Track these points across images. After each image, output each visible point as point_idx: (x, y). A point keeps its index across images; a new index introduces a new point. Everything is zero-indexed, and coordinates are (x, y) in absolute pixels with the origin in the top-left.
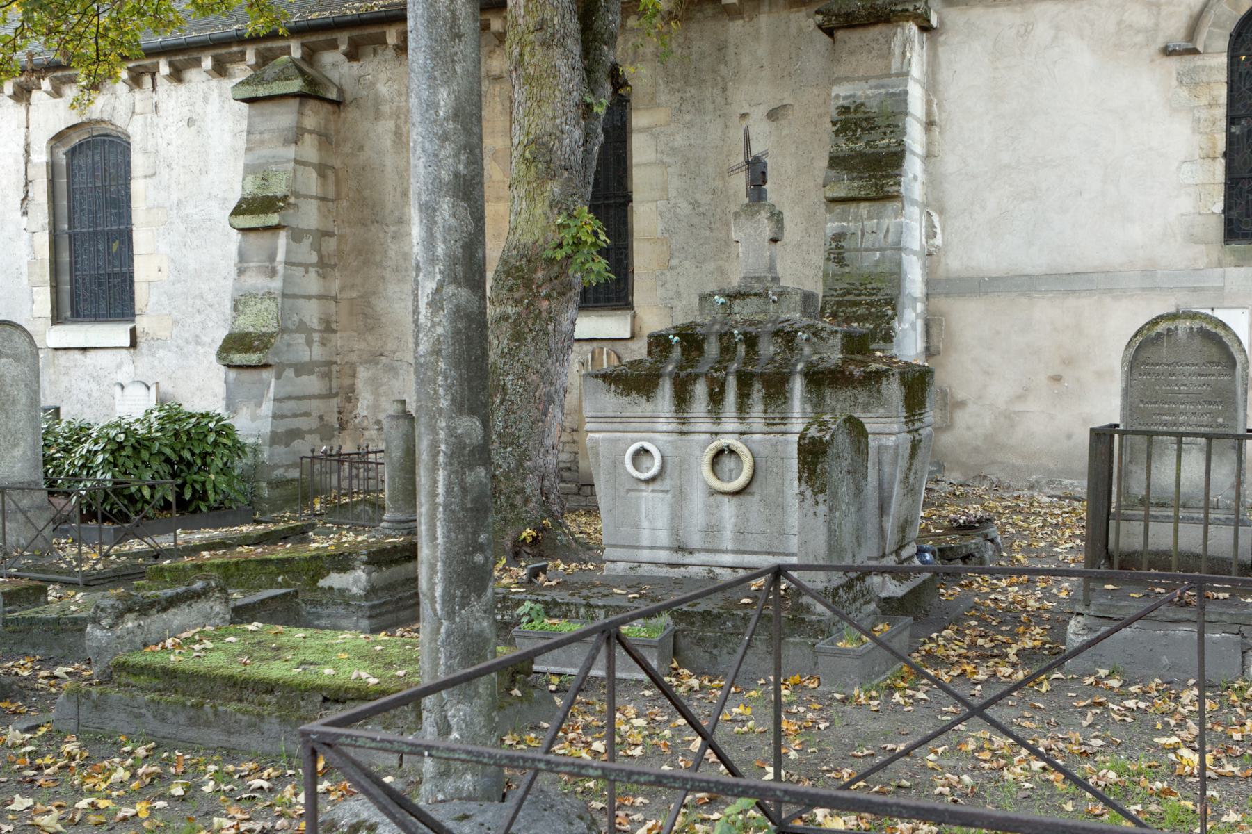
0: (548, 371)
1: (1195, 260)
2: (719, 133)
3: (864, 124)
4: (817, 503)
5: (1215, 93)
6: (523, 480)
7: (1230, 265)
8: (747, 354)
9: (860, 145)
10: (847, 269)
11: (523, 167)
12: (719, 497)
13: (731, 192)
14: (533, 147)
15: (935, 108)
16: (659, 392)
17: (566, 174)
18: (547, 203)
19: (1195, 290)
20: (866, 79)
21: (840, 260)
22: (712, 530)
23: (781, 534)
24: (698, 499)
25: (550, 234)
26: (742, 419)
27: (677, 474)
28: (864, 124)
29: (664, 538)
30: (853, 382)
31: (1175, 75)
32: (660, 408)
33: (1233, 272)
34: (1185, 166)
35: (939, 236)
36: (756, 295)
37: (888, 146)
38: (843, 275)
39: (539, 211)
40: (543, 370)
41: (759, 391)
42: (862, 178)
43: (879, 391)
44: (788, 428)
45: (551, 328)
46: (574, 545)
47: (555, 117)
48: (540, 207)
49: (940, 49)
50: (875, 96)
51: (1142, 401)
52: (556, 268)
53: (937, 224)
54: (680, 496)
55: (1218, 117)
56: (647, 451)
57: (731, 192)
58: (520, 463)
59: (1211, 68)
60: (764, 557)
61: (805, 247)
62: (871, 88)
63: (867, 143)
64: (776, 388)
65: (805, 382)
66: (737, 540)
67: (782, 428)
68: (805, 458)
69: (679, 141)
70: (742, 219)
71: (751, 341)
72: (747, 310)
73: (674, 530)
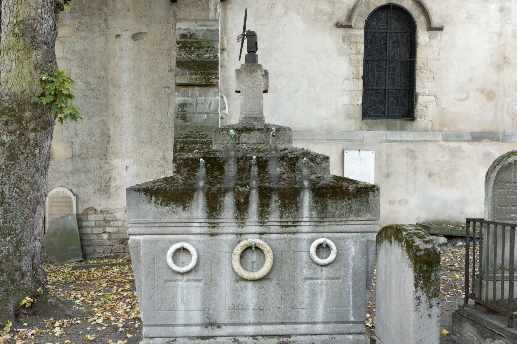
0: (36, 181)
1: (350, 126)
2: (103, 44)
4: (431, 306)
5: (359, 48)
6: (20, 260)
7: (365, 130)
8: (259, 174)
9: (194, 56)
10: (188, 123)
11: (14, 40)
12: (243, 283)
14: (21, 26)
15: (225, 42)
16: (194, 203)
17: (45, 47)
18: (32, 65)
19: (351, 141)
20: (196, 21)
21: (184, 118)
22: (237, 309)
23: (292, 308)
24: (226, 284)
25: (35, 87)
26: (262, 223)
27: (208, 266)
28: (195, 45)
29: (197, 317)
30: (348, 195)
32: (195, 215)
33: (367, 133)
34: (345, 81)
35: (227, 109)
36: (259, 130)
37: (209, 58)
38: (186, 126)
39: (25, 71)
40: (32, 181)
41: (276, 201)
42: (197, 74)
43: (367, 201)
44: (299, 228)
45: (37, 151)
46: (61, 305)
47: (37, 8)
48: (27, 68)
49: (228, 11)
50: (201, 30)
51: (499, 205)
52: (39, 111)
53: (226, 102)
54: (211, 283)
55: (360, 59)
56: (185, 250)
57: (110, 78)
58: (17, 248)
59: (357, 36)
60: (279, 326)
61: (153, 111)
62: (198, 26)
63: (197, 55)
64: (290, 199)
66: (257, 315)
67: (293, 229)
68: (421, 267)
69: (78, 46)
70: (243, 75)
71: (262, 164)
72: (252, 141)
73: (205, 311)
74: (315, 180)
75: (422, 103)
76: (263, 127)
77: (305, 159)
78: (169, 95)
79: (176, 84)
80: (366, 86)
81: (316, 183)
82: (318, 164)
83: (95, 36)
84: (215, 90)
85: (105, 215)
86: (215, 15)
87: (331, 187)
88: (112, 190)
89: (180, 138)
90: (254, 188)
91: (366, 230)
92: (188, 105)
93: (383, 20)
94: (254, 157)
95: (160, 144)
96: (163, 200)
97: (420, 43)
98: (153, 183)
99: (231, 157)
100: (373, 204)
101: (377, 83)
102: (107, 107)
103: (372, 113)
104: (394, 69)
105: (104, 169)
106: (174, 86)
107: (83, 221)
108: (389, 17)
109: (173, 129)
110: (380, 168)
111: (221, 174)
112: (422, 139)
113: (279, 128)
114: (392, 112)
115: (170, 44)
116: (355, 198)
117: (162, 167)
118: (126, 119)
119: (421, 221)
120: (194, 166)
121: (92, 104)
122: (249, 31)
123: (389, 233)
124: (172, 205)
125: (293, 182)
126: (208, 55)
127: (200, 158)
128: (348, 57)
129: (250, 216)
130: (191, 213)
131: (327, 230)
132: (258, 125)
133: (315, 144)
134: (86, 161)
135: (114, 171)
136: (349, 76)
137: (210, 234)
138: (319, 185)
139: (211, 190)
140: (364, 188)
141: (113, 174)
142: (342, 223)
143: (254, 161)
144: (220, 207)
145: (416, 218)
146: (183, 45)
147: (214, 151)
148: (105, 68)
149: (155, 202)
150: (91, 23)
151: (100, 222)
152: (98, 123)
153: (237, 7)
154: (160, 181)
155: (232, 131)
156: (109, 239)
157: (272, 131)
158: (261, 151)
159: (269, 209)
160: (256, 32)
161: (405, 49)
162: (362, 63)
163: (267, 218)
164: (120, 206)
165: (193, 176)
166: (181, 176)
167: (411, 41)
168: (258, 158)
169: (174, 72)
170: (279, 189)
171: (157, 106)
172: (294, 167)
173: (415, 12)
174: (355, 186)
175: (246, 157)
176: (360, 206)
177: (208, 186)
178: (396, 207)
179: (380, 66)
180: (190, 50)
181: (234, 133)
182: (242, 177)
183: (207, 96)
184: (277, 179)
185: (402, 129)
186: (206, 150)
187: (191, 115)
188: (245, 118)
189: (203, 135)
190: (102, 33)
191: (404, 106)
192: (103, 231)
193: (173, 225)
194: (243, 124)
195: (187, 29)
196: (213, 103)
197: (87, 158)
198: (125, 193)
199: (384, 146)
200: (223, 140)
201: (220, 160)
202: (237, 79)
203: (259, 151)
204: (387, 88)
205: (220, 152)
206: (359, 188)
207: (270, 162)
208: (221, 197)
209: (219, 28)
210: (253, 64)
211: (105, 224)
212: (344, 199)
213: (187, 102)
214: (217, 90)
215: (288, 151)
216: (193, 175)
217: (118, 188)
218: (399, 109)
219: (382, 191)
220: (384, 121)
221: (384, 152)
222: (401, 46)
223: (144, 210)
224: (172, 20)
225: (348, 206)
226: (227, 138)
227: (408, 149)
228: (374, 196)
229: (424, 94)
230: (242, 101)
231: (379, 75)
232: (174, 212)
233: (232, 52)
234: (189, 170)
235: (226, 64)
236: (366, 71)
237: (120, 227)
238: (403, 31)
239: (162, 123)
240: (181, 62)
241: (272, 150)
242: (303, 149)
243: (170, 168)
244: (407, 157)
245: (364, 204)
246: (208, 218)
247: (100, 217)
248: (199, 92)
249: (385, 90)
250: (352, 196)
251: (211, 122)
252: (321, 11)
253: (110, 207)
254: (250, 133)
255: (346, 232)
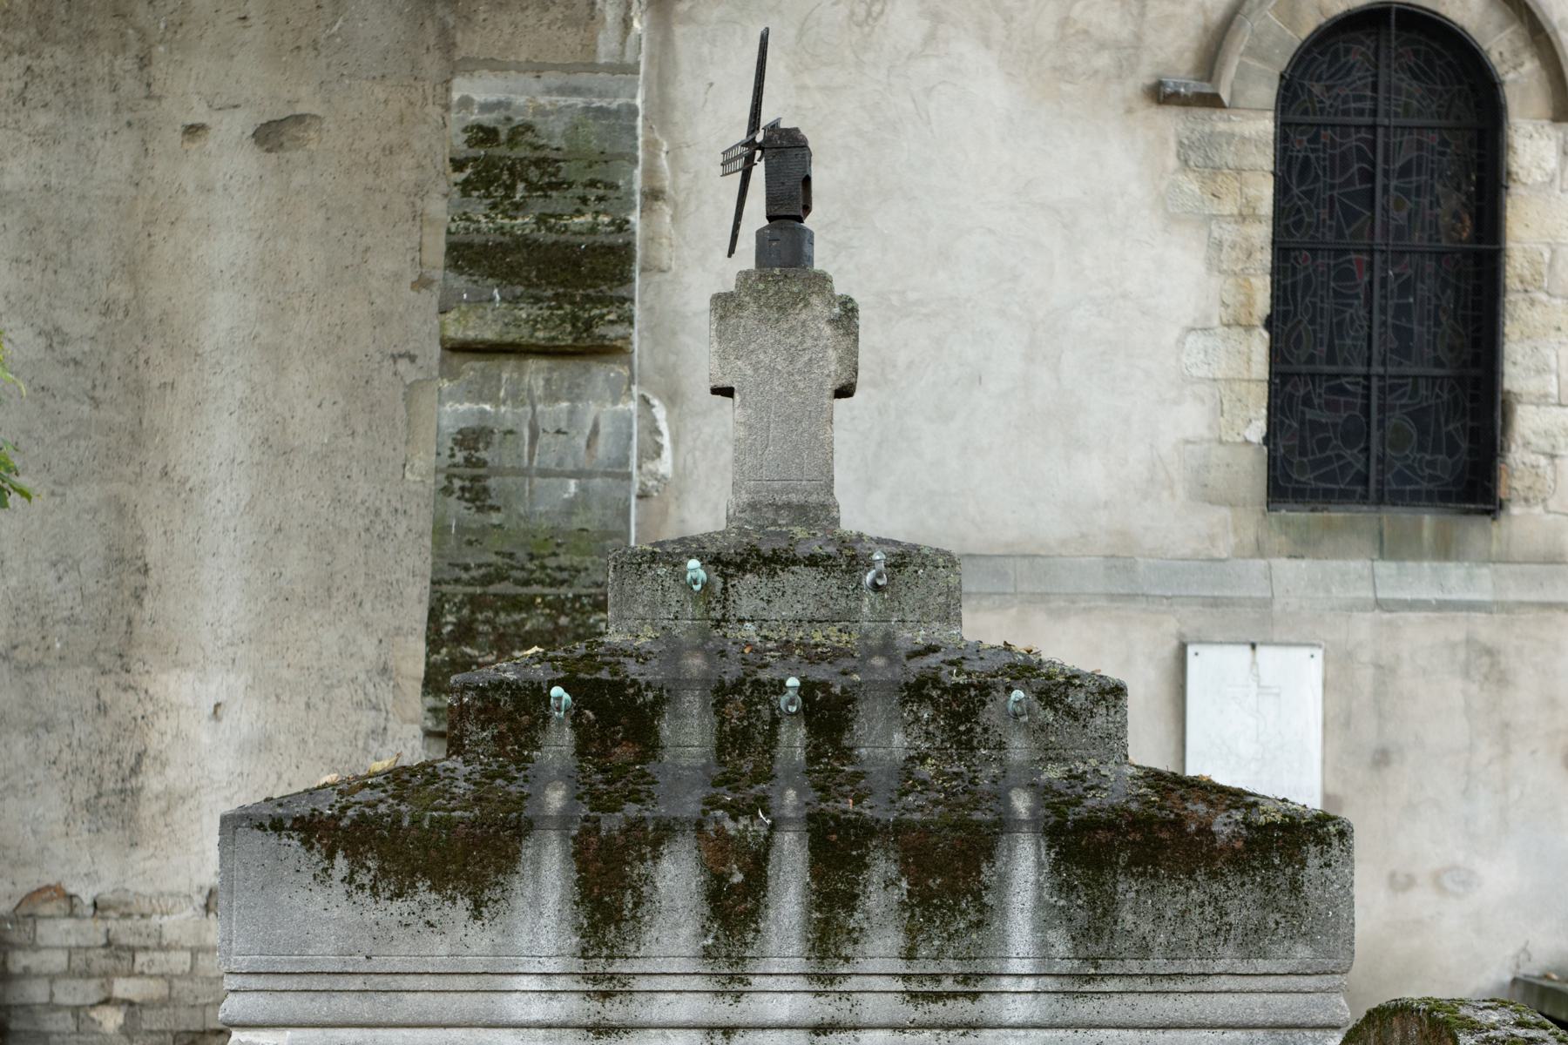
1: (1212, 539)
2: (127, 164)
3: (533, 174)
5: (1251, 192)
7: (1279, 554)
8: (814, 757)
9: (524, 223)
10: (495, 518)
13: (153, 313)
15: (664, 161)
16: (522, 886)
19: (1215, 603)
20: (538, 70)
21: (477, 495)
26: (822, 980)
28: (533, 174)
30: (1210, 859)
31: (1173, 145)
32: (523, 941)
33: (1287, 569)
34: (1191, 338)
35: (667, 454)
36: (813, 561)
37: (593, 230)
38: (484, 530)
41: (889, 883)
42: (537, 300)
43: (1295, 888)
44: (988, 1007)
49: (679, 31)
50: (560, 111)
53: (663, 426)
55: (1258, 243)
57: (153, 313)
59: (1244, 140)
61: (340, 461)
62: (548, 92)
63: (541, 220)
64: (948, 875)
65: (1048, 857)
71: (828, 715)
72: (782, 610)
74: (1061, 786)
75: (1533, 439)
76: (831, 549)
77: (1018, 694)
78: (411, 392)
79: (443, 342)
80: (1285, 361)
81: (1068, 804)
82: (1076, 719)
83: (96, 128)
84: (617, 370)
85: (112, 924)
86: (623, 43)
87: (1136, 822)
88: (149, 810)
89: (457, 581)
90: (790, 821)
91: (1289, 1020)
92: (497, 438)
93: (1356, 74)
94: (793, 682)
95: (367, 606)
96: (384, 873)
97: (1522, 175)
98: (341, 793)
99: (689, 682)
100: (1321, 899)
101: (1331, 347)
102: (136, 440)
103: (1308, 478)
104: (1406, 287)
105: (114, 715)
106: (437, 351)
107: (14, 946)
108: (1382, 55)
109: (428, 542)
110: (1347, 724)
111: (643, 758)
112: (1533, 596)
113: (903, 556)
114: (1402, 478)
115: (420, 166)
116: (1243, 872)
117: (376, 708)
118: (217, 493)
119: (1532, 969)
120: (525, 719)
121: (71, 428)
122: (774, 127)
123: (1397, 1036)
124: (424, 893)
125: (964, 798)
126: (588, 218)
127: (552, 684)
128: (1204, 233)
129: (772, 948)
130: (507, 932)
131: (1117, 1017)
132: (809, 541)
133: (1058, 615)
134: (38, 677)
135: (161, 723)
136: (1208, 318)
137: (588, 1029)
138: (1082, 812)
139: (598, 830)
140: (1281, 826)
141: (154, 736)
142: (1180, 987)
143: (792, 702)
144: (636, 905)
145: (1511, 951)
146: (477, 173)
147: (614, 651)
148: (132, 268)
149: (349, 879)
150: (79, 74)
151: (91, 954)
152: (95, 511)
153: (716, 13)
154: (373, 787)
155: (694, 563)
156: (127, 1030)
157: (870, 565)
158: (822, 658)
159: (858, 915)
160: (803, 132)
161: (1453, 201)
162: (1265, 258)
163: (847, 959)
164: (179, 883)
165: (517, 762)
166: (466, 762)
167: (1480, 167)
168: (807, 688)
169: (435, 288)
170: (900, 828)
171: (359, 440)
172: (970, 730)
173: (1499, 43)
174: (1238, 816)
175: (757, 684)
176: (1263, 906)
177: (585, 811)
178: (1421, 900)
179: (1345, 274)
180: (507, 197)
181: (702, 575)
182: (737, 770)
183: (579, 397)
184: (894, 784)
185: (1445, 550)
186: (580, 648)
187: (509, 480)
188: (753, 506)
189: (560, 569)
190: (127, 116)
191: (1452, 449)
192: (103, 995)
193: (426, 982)
194: (742, 532)
195: (499, 105)
196: (605, 429)
197: (40, 665)
198: (217, 839)
199: (1363, 627)
200: (652, 605)
201: (639, 692)
202: (720, 335)
203: (814, 656)
204: (1377, 369)
205: (641, 657)
206: (1259, 828)
207: (862, 707)
208: (642, 859)
209: (639, 102)
210: (791, 272)
211: (111, 962)
212: (1190, 874)
213: (490, 424)
214: (625, 372)
215: (940, 656)
216: (521, 761)
217: (173, 800)
218: (1432, 464)
219: (1360, 840)
220: (1364, 517)
221: (1365, 656)
222: (1438, 188)
223: (298, 916)
224: (432, 65)
225: (1209, 910)
226: (673, 597)
227: (1470, 642)
228: (1328, 865)
229: (1542, 400)
230: (742, 433)
231: (1338, 312)
232: (429, 924)
233: (692, 207)
234: (499, 739)
235: (665, 256)
236: (1280, 293)
237: (181, 977)
238: (1443, 122)
239: (377, 513)
240: (470, 246)
241: (871, 653)
242: (1007, 647)
243: (410, 714)
244: (1466, 674)
245: (1284, 899)
246: (584, 953)
247: (92, 931)
248: (548, 381)
249: (1367, 377)
250: (1229, 861)
251: (597, 511)
252: (1086, 32)
253: (136, 885)
254: (772, 574)
255: (1204, 1027)
